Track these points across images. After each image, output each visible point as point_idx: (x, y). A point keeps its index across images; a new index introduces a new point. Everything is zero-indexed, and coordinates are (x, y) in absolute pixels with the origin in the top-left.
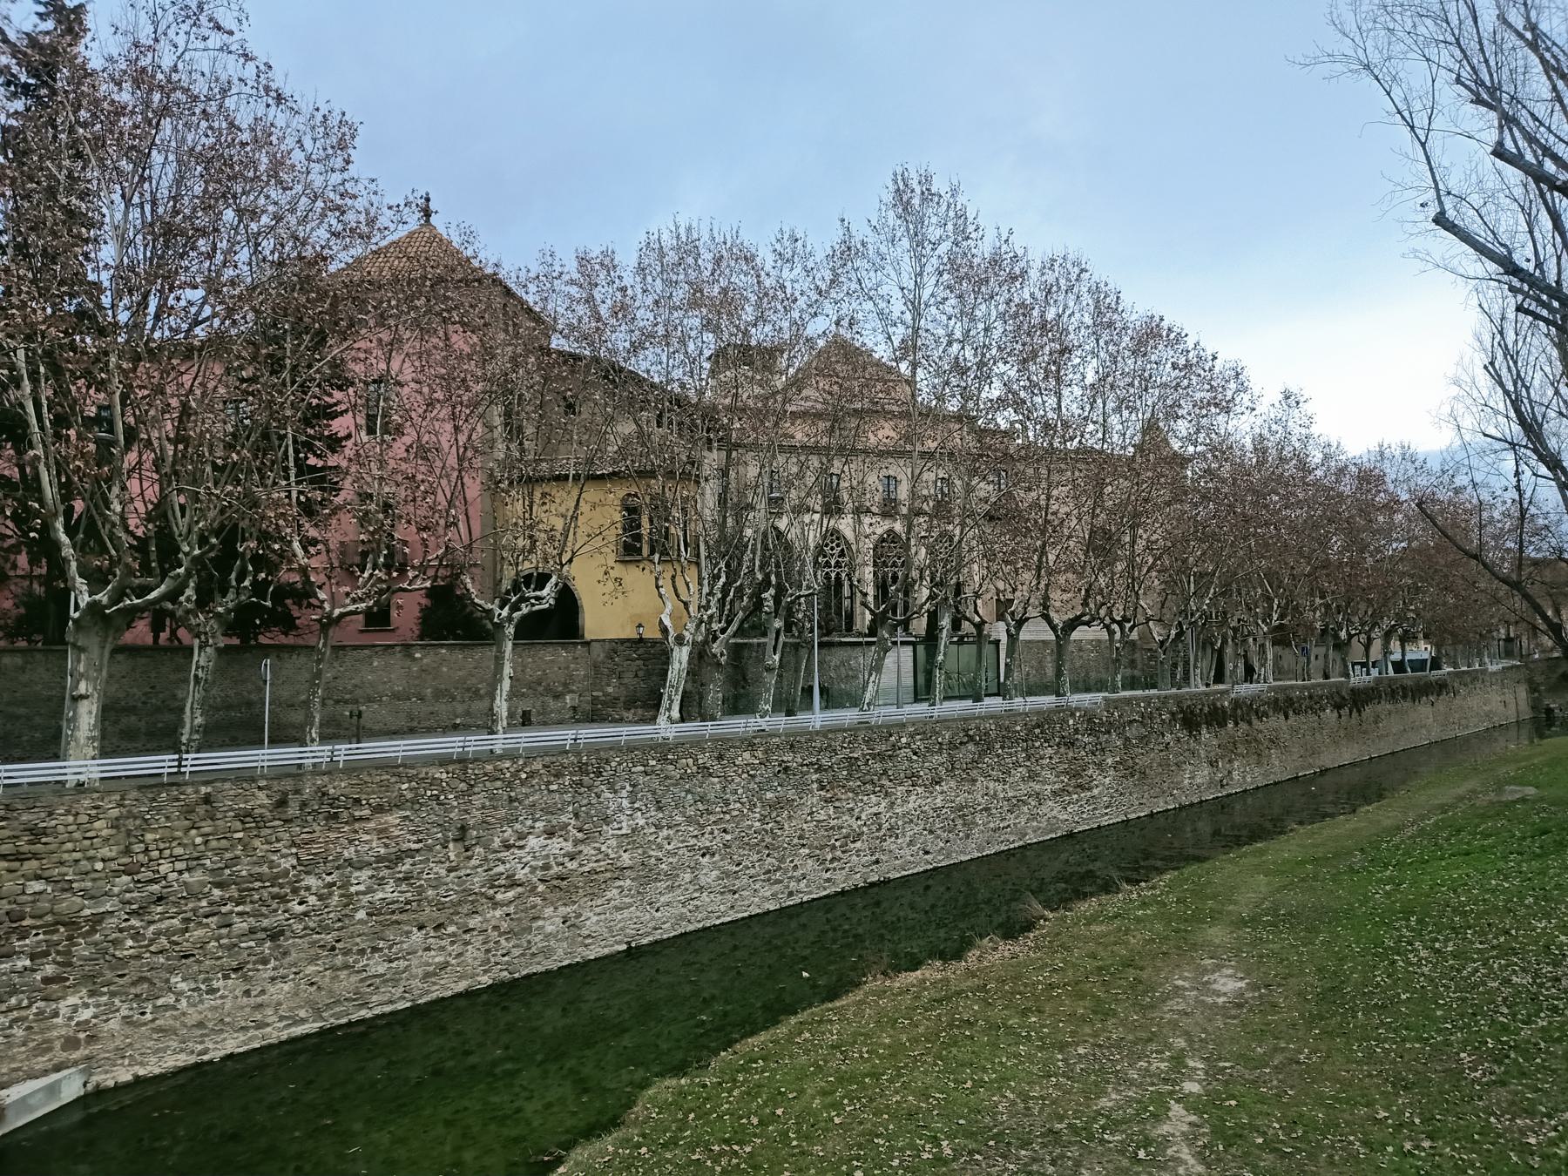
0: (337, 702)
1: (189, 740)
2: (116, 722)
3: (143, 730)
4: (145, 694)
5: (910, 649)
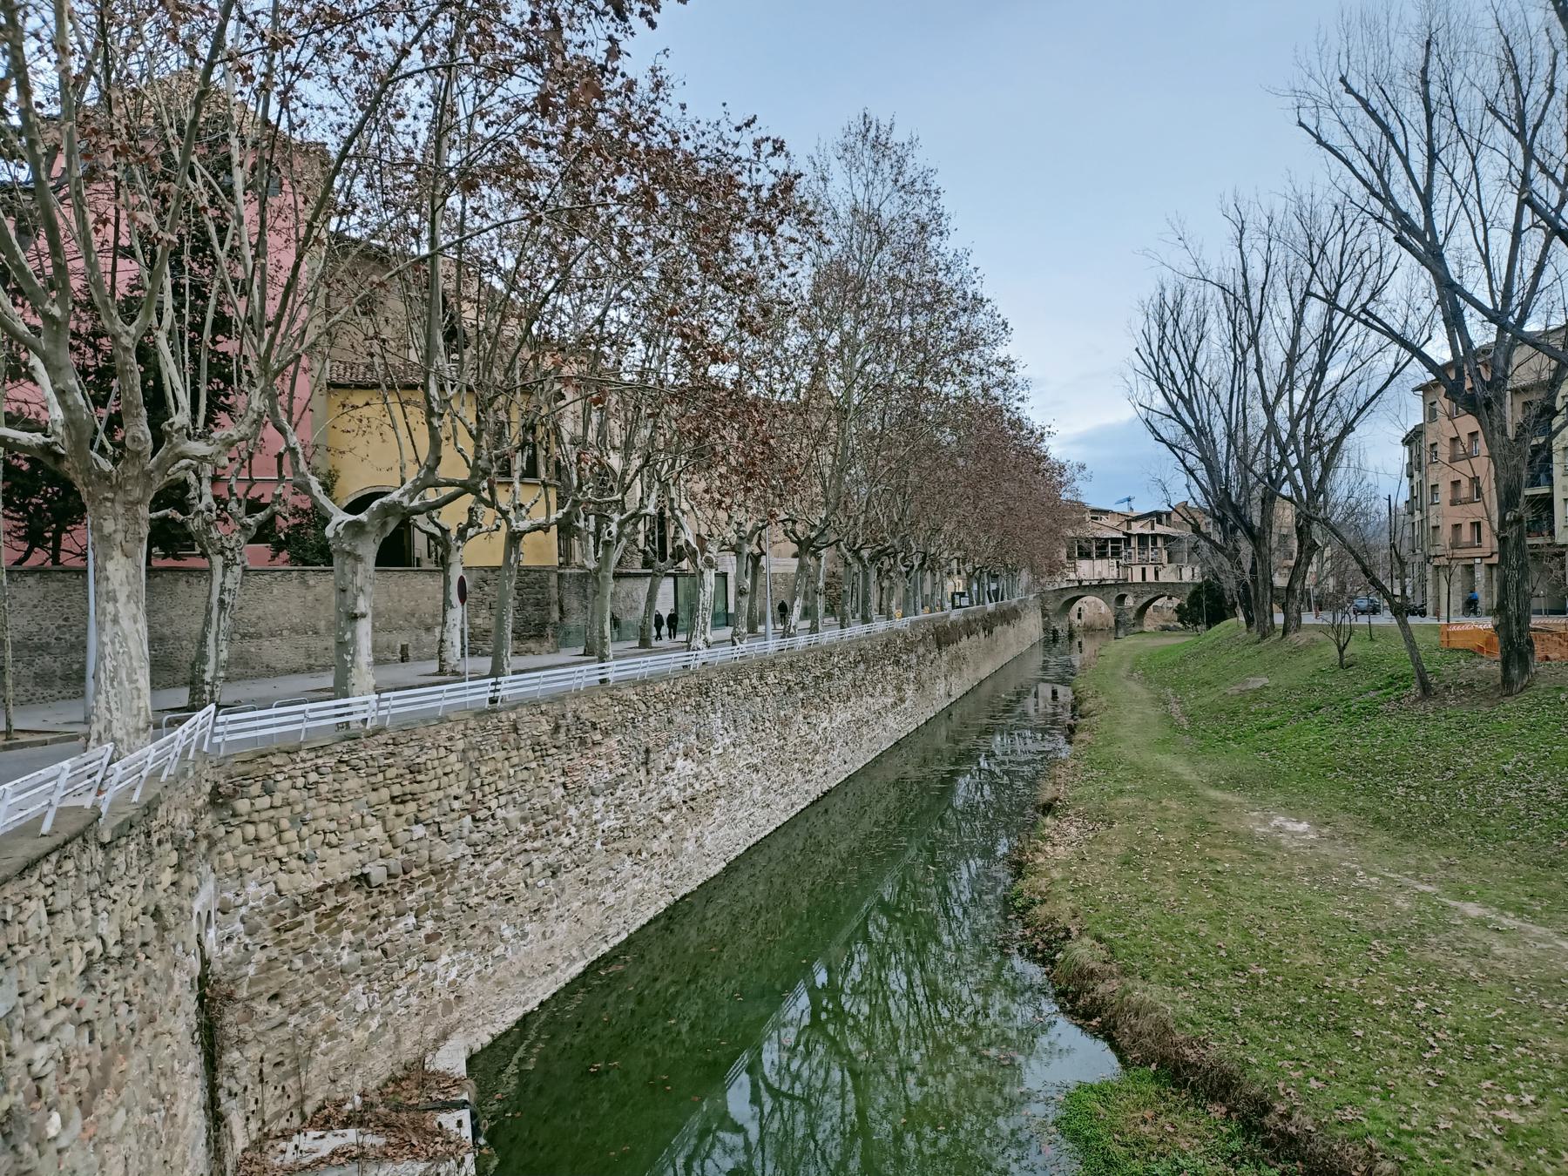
0: (243, 636)
1: (215, 678)
2: (30, 664)
3: (59, 673)
4: (58, 628)
5: (671, 580)
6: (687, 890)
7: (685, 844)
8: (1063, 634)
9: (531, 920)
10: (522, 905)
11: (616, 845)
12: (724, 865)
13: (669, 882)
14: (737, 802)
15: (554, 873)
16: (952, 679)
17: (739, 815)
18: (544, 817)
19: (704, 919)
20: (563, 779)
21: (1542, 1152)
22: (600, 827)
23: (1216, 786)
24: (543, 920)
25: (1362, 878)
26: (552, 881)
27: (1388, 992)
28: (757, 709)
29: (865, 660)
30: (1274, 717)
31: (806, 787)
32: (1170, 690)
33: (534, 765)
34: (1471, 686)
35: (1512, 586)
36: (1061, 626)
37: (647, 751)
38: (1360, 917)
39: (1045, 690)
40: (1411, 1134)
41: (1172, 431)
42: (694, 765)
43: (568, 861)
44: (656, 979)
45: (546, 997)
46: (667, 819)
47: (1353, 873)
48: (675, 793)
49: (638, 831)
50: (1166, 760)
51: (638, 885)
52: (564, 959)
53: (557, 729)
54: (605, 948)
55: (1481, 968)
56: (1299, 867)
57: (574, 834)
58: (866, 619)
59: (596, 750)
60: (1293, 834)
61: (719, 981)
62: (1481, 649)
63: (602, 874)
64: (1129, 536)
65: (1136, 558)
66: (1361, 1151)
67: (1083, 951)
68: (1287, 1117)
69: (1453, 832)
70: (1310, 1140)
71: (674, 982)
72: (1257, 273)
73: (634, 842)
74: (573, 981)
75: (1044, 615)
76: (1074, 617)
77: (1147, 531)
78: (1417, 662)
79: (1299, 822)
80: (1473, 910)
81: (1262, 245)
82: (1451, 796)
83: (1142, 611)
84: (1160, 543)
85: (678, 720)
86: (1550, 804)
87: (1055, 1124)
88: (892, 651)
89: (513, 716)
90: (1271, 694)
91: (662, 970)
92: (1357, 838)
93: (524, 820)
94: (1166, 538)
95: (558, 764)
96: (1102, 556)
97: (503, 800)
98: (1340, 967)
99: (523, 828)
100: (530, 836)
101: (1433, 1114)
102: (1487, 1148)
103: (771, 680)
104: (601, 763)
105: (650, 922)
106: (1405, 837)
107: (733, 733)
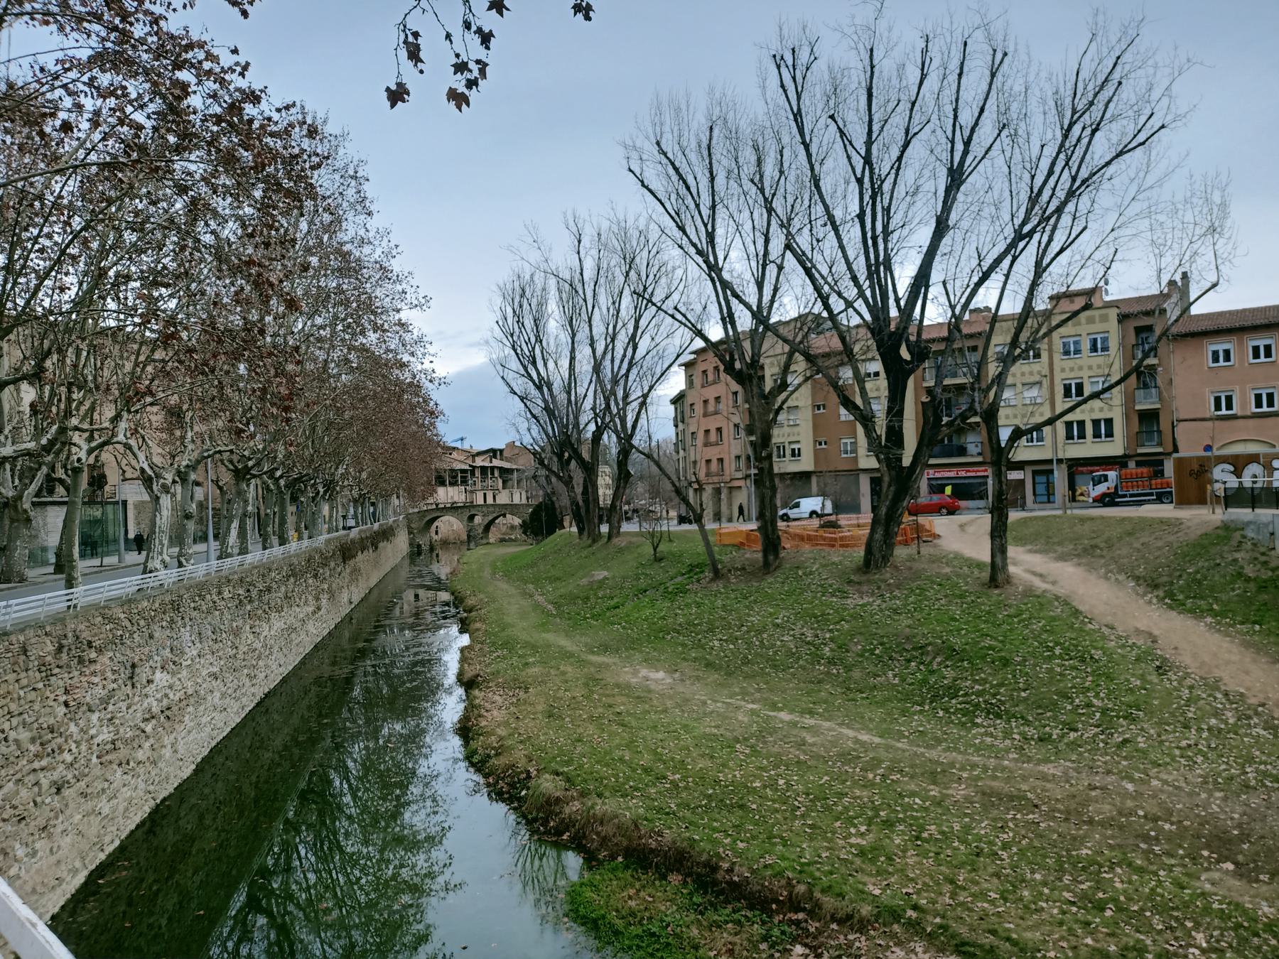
6: (165, 794)
7: (164, 751)
8: (425, 548)
9: (40, 838)
10: (33, 823)
11: (109, 757)
12: (193, 767)
13: (151, 788)
14: (202, 708)
15: (59, 790)
16: (353, 588)
17: (204, 720)
18: (50, 736)
19: (178, 819)
20: (65, 698)
21: (883, 859)
22: (96, 741)
23: (593, 653)
24: (50, 836)
25: (711, 706)
26: (56, 798)
27: (760, 778)
28: (216, 622)
29: (294, 575)
30: (616, 600)
31: (252, 690)
32: (531, 586)
33: (40, 685)
34: (744, 569)
35: (767, 500)
36: (423, 541)
37: (134, 666)
38: (722, 731)
39: (409, 596)
40: (808, 864)
41: (521, 384)
42: (169, 677)
43: (70, 776)
44: (142, 880)
45: (56, 910)
46: (149, 728)
47: (704, 703)
48: (155, 703)
49: (126, 742)
50: (550, 637)
51: (126, 793)
52: (70, 871)
53: (60, 649)
54: (102, 856)
55: (805, 753)
56: (669, 703)
57: (74, 750)
58: (283, 541)
59: (93, 668)
60: (656, 681)
61: (189, 874)
62: (742, 544)
63: (99, 785)
64: (474, 467)
65: (479, 485)
66: (783, 882)
67: (548, 785)
68: (730, 871)
69: (756, 667)
70: (748, 883)
71: (155, 881)
72: (589, 274)
73: (123, 753)
74: (78, 891)
75: (410, 533)
76: (433, 534)
77: (487, 464)
78: (710, 553)
79: (657, 671)
80: (784, 716)
81: (594, 252)
82: (749, 644)
83: (487, 528)
84: (496, 474)
85: (156, 635)
86: (808, 643)
87: (566, 915)
88: (313, 566)
89: (22, 638)
90: (610, 582)
91: (147, 870)
92: (698, 678)
93: (33, 740)
94: (501, 469)
95: (61, 683)
96: (452, 484)
97: (15, 721)
98: (724, 765)
99: (32, 748)
100: (38, 756)
101: (816, 850)
102: (852, 863)
103: (226, 595)
104: (96, 680)
105: (138, 827)
106: (729, 674)
107: (198, 645)
